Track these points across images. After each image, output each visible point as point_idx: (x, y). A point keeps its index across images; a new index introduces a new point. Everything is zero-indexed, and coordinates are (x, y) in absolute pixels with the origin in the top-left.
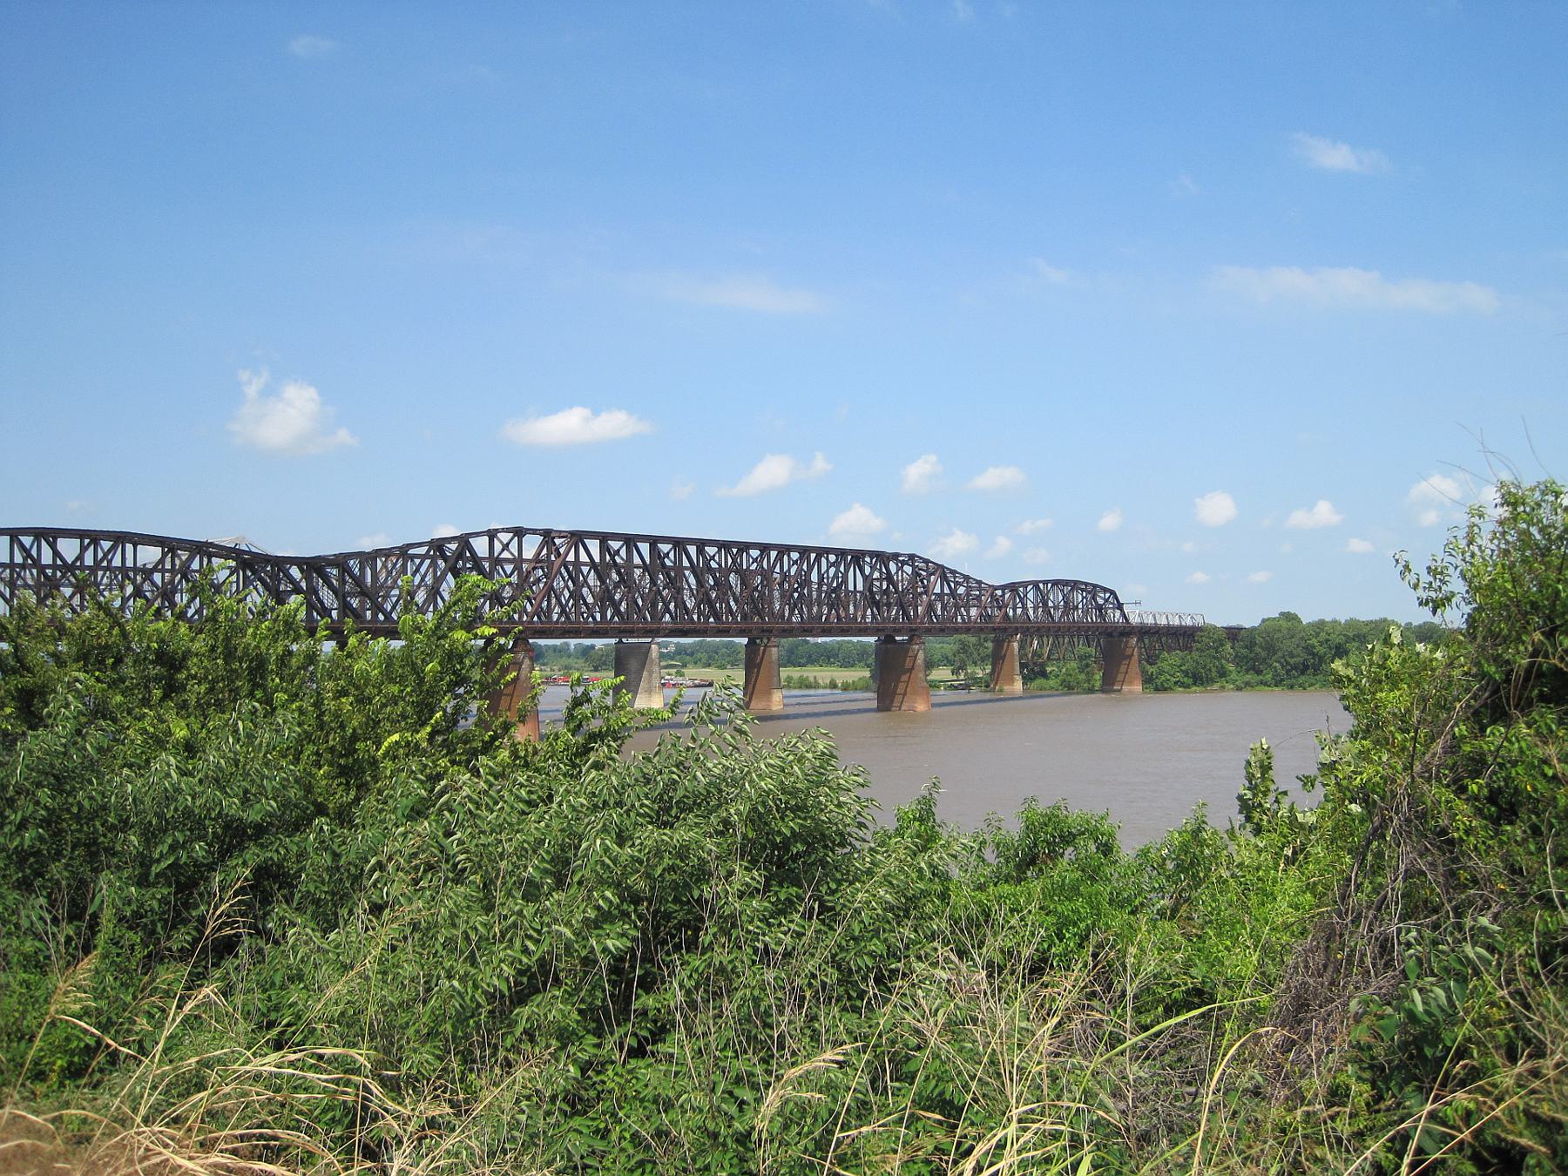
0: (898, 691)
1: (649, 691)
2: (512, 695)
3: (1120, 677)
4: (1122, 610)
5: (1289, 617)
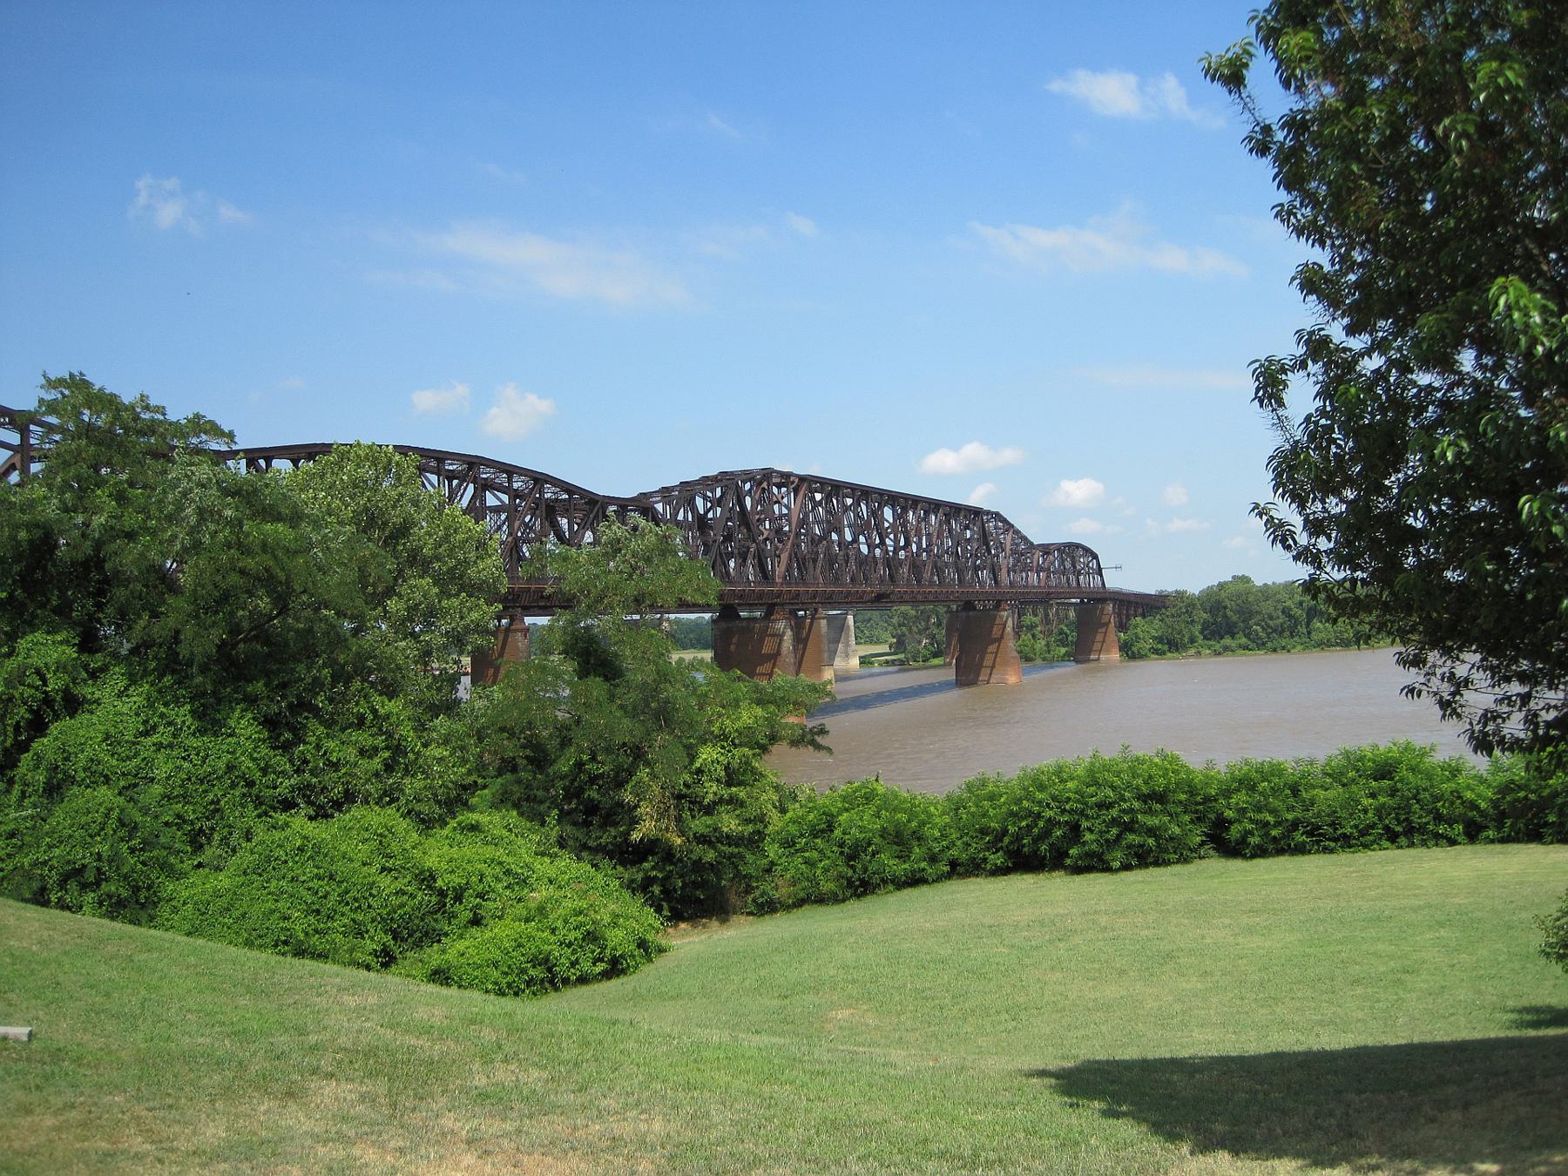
2: (997, 653)
3: (1097, 646)
4: (1101, 576)
5: (1245, 579)
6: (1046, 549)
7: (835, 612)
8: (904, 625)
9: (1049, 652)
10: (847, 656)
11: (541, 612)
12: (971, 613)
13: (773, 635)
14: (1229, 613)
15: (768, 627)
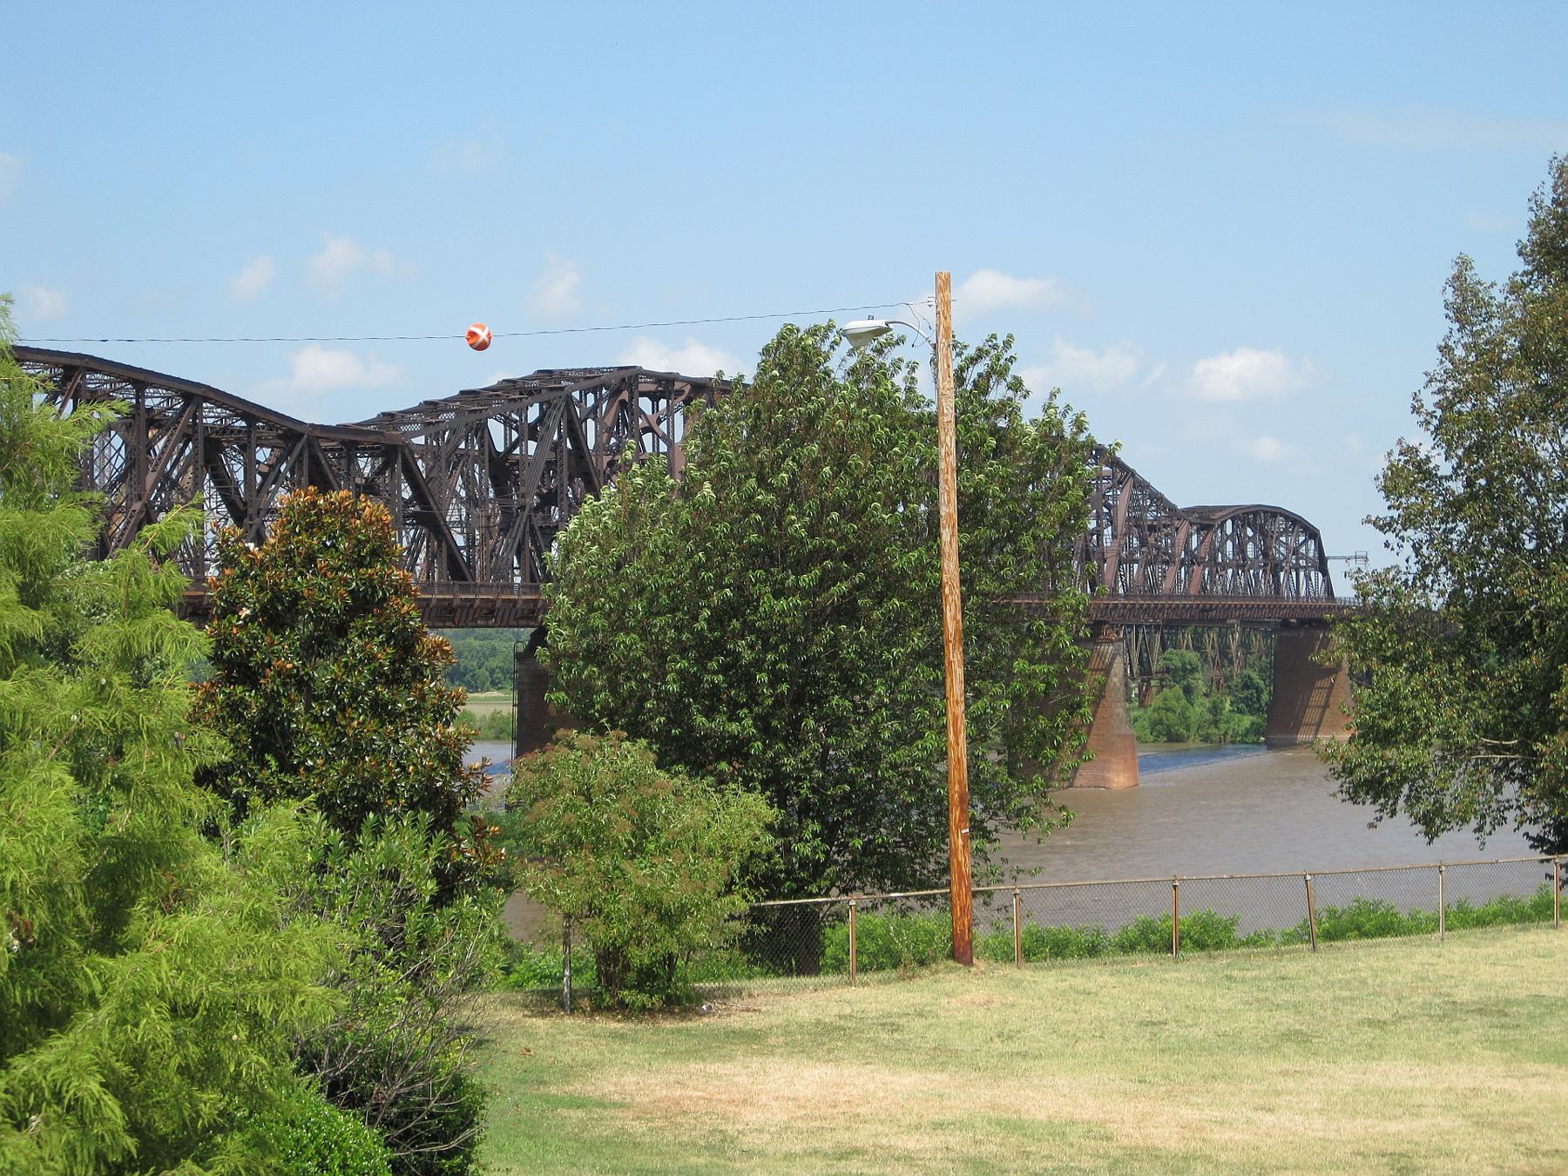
3: (1311, 715)
4: (1325, 573)
6: (1205, 519)
9: (1216, 723)
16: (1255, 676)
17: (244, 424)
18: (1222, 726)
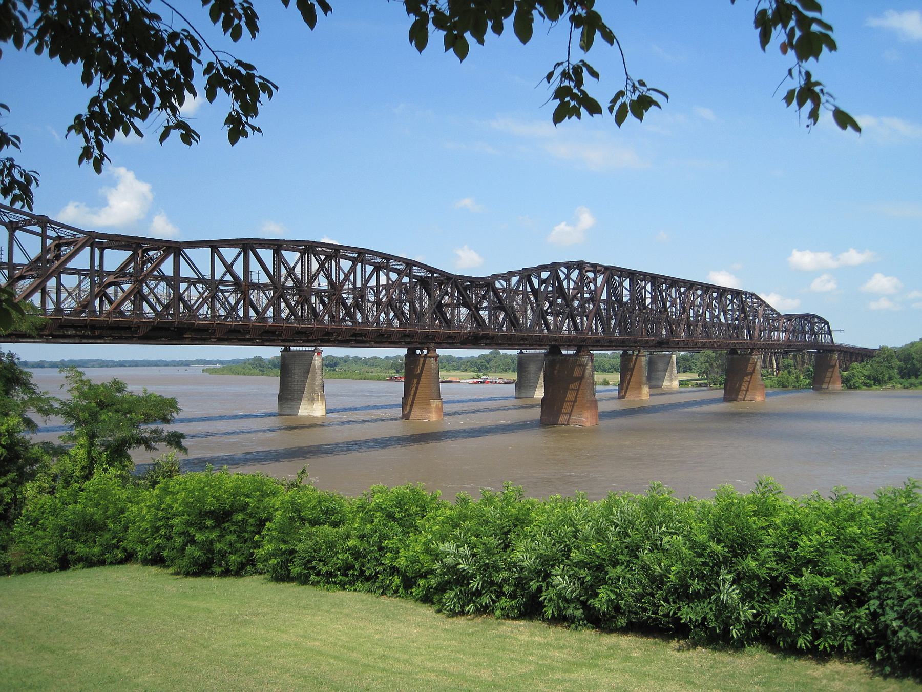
0: (743, 388)
1: (312, 400)
2: (578, 390)
3: (827, 380)
4: (831, 335)
6: (789, 317)
7: (667, 353)
8: (708, 362)
9: (797, 382)
10: (671, 380)
11: (448, 346)
12: (734, 356)
13: (580, 365)
14: (915, 362)
15: (577, 360)
16: (811, 368)
17: (112, 11)
18: (800, 383)
